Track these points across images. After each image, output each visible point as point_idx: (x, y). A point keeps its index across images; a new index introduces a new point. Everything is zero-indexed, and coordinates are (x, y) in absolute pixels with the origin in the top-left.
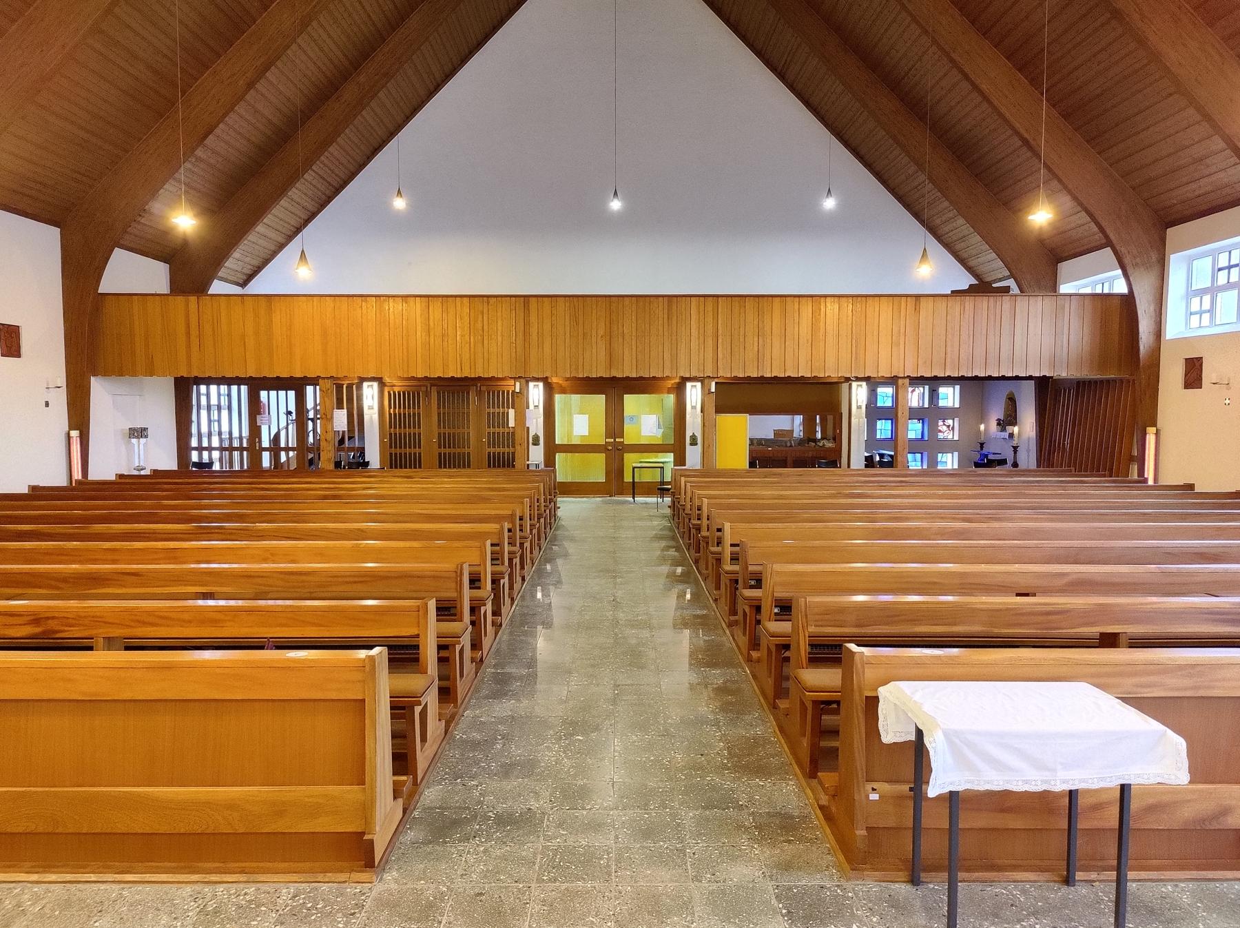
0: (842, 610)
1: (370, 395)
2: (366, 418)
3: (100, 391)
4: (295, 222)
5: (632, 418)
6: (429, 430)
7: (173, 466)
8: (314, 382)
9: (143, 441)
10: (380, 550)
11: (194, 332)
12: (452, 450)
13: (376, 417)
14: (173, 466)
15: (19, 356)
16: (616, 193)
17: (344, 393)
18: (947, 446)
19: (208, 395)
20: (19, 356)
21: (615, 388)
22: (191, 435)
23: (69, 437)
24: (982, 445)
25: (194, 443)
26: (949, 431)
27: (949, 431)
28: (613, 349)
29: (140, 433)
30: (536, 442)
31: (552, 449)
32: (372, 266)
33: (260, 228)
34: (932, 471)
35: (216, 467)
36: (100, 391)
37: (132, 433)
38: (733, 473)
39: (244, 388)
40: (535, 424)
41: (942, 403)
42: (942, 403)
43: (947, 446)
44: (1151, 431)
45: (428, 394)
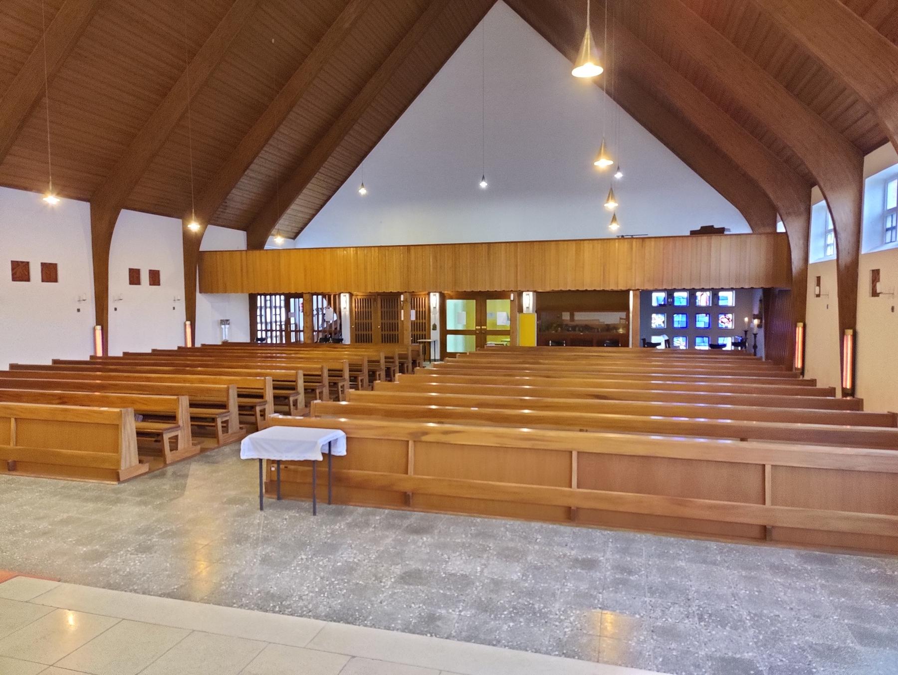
0: (439, 423)
1: (344, 301)
2: (343, 313)
3: (202, 301)
4: (319, 202)
5: (491, 314)
6: (377, 322)
7: (248, 340)
8: (298, 296)
9: (227, 326)
10: (100, 376)
11: (244, 270)
12: (391, 333)
13: (348, 313)
14: (248, 340)
15: (159, 284)
16: (483, 177)
17: (333, 300)
18: (726, 333)
19: (271, 300)
20: (159, 284)
21: (481, 298)
22: (257, 323)
23: (185, 325)
24: (746, 332)
25: (259, 327)
26: (726, 322)
27: (726, 322)
28: (473, 273)
29: (225, 322)
30: (435, 328)
31: (445, 332)
32: (365, 222)
33: (293, 206)
34: (716, 347)
35: (269, 341)
36: (202, 301)
37: (222, 321)
38: (530, 349)
39: (283, 297)
40: (435, 318)
41: (721, 303)
42: (721, 303)
43: (726, 333)
44: (800, 325)
45: (375, 300)
